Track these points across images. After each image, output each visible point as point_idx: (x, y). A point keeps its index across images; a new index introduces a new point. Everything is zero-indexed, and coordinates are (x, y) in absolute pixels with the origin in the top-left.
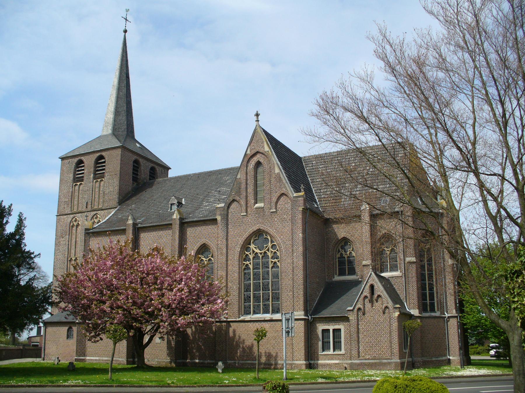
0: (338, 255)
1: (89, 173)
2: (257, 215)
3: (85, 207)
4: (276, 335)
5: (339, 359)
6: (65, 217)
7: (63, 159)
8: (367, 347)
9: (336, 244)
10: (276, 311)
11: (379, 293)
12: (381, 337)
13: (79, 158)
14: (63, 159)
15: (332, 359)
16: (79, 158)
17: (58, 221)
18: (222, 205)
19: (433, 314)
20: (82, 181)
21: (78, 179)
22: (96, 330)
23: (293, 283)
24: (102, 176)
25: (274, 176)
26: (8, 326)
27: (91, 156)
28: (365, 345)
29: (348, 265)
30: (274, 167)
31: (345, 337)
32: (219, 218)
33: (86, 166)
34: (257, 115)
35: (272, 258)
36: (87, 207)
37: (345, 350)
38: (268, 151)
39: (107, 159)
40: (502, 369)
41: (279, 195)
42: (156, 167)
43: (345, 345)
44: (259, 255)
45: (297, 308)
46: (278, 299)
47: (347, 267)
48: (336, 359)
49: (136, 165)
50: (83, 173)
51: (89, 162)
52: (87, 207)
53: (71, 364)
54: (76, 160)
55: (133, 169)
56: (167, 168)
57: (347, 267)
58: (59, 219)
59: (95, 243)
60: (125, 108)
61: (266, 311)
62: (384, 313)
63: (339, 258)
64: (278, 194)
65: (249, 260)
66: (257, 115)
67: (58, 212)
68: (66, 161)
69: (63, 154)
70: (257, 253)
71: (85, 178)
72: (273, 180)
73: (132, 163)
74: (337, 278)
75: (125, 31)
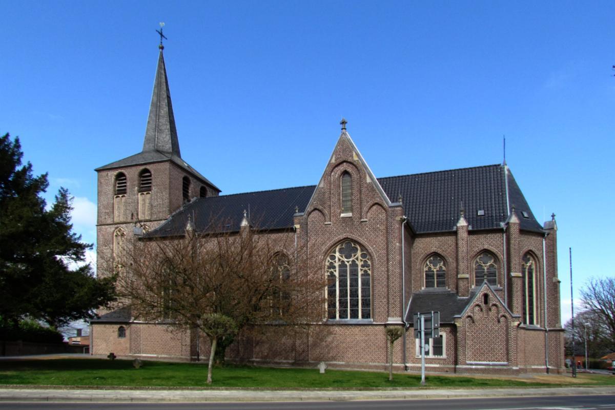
0: (426, 269)
1: (133, 186)
2: (344, 225)
4: (367, 338)
5: (439, 363)
6: (107, 227)
8: (477, 353)
9: (424, 259)
12: (496, 344)
13: (120, 171)
15: (431, 363)
16: (120, 171)
17: (99, 231)
20: (125, 193)
21: (121, 191)
22: (601, 331)
23: (388, 290)
24: (149, 189)
26: (37, 316)
27: (134, 169)
28: (475, 351)
29: (437, 279)
30: (365, 176)
31: (447, 342)
33: (128, 179)
35: (362, 266)
36: (132, 219)
37: (448, 355)
38: (358, 161)
39: (152, 173)
41: (371, 204)
42: (207, 188)
43: (447, 350)
44: (346, 263)
45: (391, 313)
46: (368, 305)
47: (436, 280)
48: (435, 363)
49: (185, 182)
50: (125, 186)
51: (132, 175)
52: (132, 219)
53: (112, 355)
54: (116, 172)
55: (183, 186)
57: (436, 280)
58: (100, 229)
60: (168, 127)
63: (426, 271)
64: (371, 203)
65: (334, 267)
67: (98, 222)
68: (104, 173)
71: (128, 191)
72: (364, 190)
73: (182, 179)
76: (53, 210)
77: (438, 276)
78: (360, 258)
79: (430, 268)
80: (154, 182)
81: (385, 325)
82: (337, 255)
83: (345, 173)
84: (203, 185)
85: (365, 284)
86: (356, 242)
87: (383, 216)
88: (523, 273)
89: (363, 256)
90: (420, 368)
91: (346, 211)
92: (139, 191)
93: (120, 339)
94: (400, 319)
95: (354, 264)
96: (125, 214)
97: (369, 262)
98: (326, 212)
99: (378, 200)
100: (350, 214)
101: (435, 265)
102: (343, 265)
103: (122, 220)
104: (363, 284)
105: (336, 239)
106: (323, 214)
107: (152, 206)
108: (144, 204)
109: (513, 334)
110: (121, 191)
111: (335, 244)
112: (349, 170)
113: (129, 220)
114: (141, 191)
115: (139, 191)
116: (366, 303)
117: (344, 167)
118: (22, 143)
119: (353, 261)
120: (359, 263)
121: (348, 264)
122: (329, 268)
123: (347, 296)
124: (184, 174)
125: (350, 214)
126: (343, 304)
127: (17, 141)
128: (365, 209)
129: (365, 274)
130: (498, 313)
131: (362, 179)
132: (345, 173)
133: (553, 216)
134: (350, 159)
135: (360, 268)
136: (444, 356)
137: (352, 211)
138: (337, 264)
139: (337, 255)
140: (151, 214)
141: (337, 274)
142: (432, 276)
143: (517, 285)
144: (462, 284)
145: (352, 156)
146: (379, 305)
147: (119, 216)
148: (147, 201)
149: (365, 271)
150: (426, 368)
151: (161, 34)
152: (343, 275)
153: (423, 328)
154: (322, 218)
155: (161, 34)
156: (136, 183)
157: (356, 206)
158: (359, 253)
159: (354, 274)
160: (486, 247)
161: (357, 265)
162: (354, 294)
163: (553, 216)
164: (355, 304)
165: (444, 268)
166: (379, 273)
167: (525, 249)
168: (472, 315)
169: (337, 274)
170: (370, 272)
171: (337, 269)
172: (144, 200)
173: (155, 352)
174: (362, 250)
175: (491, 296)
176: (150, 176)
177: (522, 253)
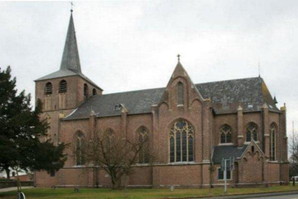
3: (54, 108)
7: (36, 81)
10: (191, 160)
11: (257, 150)
14: (36, 81)
18: (156, 105)
19: (274, 162)
24: (65, 91)
25: (190, 89)
32: (153, 112)
34: (179, 56)
35: (189, 133)
40: (246, 189)
51: (56, 86)
56: (101, 90)
59: (64, 126)
61: (184, 160)
62: (52, 187)
65: (173, 134)
66: (179, 56)
68: (39, 83)
69: (37, 78)
70: (178, 131)
71: (53, 92)
72: (190, 92)
74: (220, 144)
75: (72, 11)
76: (38, 116)
77: (228, 137)
78: (187, 129)
79: (223, 133)
80: (68, 88)
81: (202, 165)
82: (175, 127)
83: (180, 83)
84: (94, 88)
85: (191, 142)
86: (185, 120)
87: (200, 106)
88: (270, 134)
89: (189, 127)
90: (223, 186)
91: (179, 103)
92: (59, 93)
93: (51, 177)
94: (209, 160)
95: (184, 132)
96: (51, 106)
97: (193, 131)
98: (169, 104)
99: (197, 97)
100: (182, 105)
101: (225, 131)
102: (178, 133)
103: (49, 109)
104: (189, 143)
105: (175, 118)
106: (168, 106)
107: (66, 101)
108: (62, 100)
109: (266, 166)
110: (49, 93)
111: (174, 121)
112: (182, 81)
113: (54, 109)
114: (61, 92)
115: (59, 93)
116: (191, 153)
117: (178, 80)
118: (17, 80)
119: (184, 131)
120: (187, 131)
121: (181, 132)
122: (170, 134)
123: (180, 149)
124: (84, 82)
125: (182, 105)
126: (178, 154)
127: (15, 78)
128: (191, 102)
129: (190, 137)
130: (259, 155)
131: (188, 87)
132: (180, 83)
133: (285, 104)
134: (182, 75)
135: (187, 134)
136: (231, 179)
137: (183, 103)
138: (175, 132)
139: (175, 127)
140: (67, 105)
141: (175, 138)
142: (224, 137)
143: (267, 141)
144: (240, 141)
145: (183, 74)
146: (198, 152)
147: (48, 107)
148: (64, 98)
149: (190, 136)
150: (223, 182)
151: (72, 4)
152: (178, 138)
153: (225, 166)
154: (167, 107)
155: (72, 4)
156: (58, 88)
157: (186, 101)
158: (187, 126)
159: (185, 138)
160: (252, 121)
161: (186, 132)
162: (184, 148)
163: (285, 104)
164: (185, 154)
165: (230, 133)
166: (198, 137)
167: (271, 122)
168: (246, 157)
169: (175, 138)
170: (193, 136)
171: (175, 135)
172: (62, 98)
173: (73, 184)
174: (188, 125)
175: (255, 147)
176: (66, 84)
177: (270, 123)
